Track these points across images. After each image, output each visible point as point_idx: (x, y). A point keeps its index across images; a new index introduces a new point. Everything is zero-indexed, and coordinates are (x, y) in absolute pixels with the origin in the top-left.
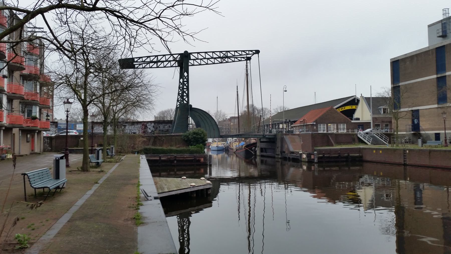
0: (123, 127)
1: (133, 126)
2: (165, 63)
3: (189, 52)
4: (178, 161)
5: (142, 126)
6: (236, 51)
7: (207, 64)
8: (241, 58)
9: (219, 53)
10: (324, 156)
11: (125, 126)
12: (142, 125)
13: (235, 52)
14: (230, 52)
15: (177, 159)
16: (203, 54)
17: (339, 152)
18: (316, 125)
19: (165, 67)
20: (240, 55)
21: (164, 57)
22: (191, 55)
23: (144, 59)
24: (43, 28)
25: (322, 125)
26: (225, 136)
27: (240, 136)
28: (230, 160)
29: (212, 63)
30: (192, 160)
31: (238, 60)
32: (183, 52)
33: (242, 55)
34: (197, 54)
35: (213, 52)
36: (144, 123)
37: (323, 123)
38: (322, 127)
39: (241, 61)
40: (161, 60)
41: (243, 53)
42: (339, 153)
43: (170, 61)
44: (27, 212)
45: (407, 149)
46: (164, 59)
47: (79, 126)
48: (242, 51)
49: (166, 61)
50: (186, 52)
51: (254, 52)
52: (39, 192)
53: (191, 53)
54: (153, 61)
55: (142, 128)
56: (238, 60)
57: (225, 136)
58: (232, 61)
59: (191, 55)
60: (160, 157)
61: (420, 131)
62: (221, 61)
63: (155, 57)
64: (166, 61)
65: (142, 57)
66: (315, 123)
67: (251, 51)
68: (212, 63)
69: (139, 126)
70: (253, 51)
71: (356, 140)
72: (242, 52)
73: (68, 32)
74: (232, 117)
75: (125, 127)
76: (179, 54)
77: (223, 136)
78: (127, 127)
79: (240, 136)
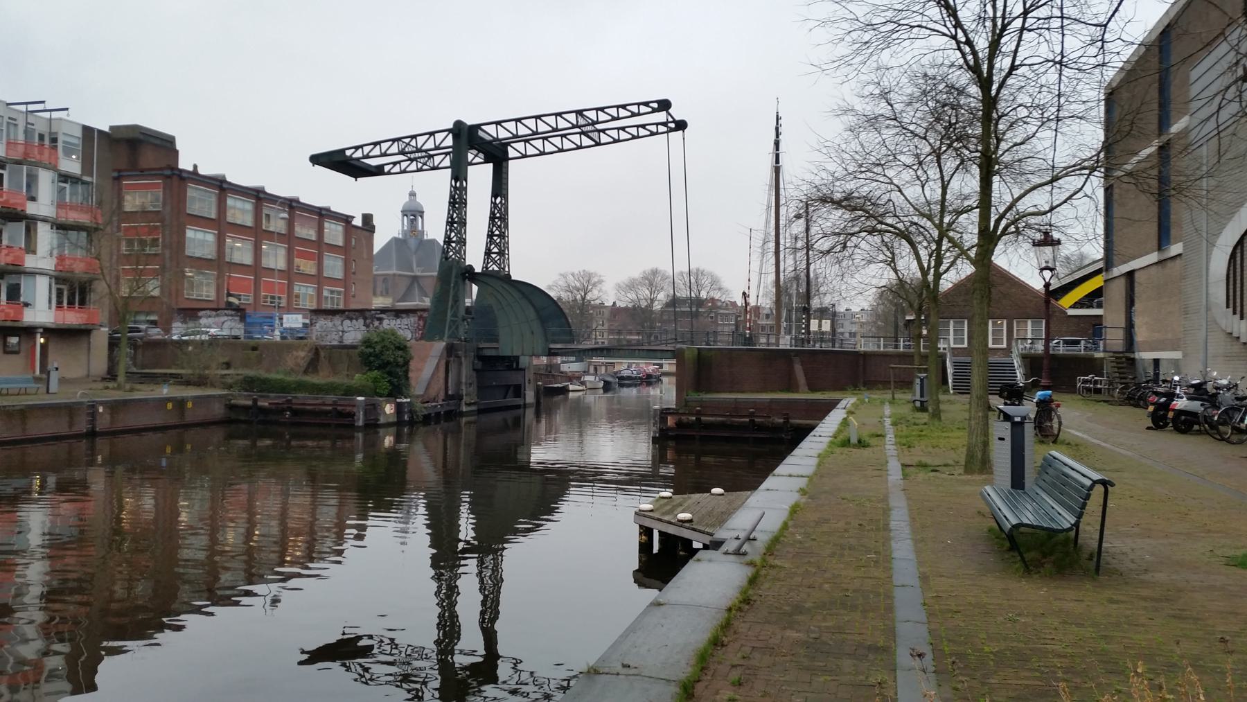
0: (376, 323)
1: (398, 321)
4: (295, 413)
5: (419, 320)
6: (602, 109)
7: (561, 150)
10: (698, 420)
11: (380, 320)
12: (417, 318)
13: (599, 112)
15: (294, 407)
16: (531, 123)
17: (751, 410)
20: (614, 119)
21: (432, 137)
24: (43, 102)
25: (1029, 322)
26: (564, 351)
27: (605, 352)
30: (329, 412)
33: (618, 118)
35: (538, 117)
36: (422, 313)
38: (1029, 328)
39: (657, 133)
42: (753, 413)
45: (102, 403)
47: (288, 318)
48: (618, 107)
51: (655, 105)
53: (478, 126)
55: (419, 325)
56: (649, 133)
57: (564, 351)
58: (630, 136)
60: (255, 401)
61: (1134, 352)
63: (391, 143)
65: (361, 147)
67: (646, 104)
69: (412, 319)
70: (651, 105)
72: (620, 109)
73: (1059, 52)
75: (380, 324)
76: (449, 131)
77: (560, 351)
78: (385, 322)
79: (605, 352)
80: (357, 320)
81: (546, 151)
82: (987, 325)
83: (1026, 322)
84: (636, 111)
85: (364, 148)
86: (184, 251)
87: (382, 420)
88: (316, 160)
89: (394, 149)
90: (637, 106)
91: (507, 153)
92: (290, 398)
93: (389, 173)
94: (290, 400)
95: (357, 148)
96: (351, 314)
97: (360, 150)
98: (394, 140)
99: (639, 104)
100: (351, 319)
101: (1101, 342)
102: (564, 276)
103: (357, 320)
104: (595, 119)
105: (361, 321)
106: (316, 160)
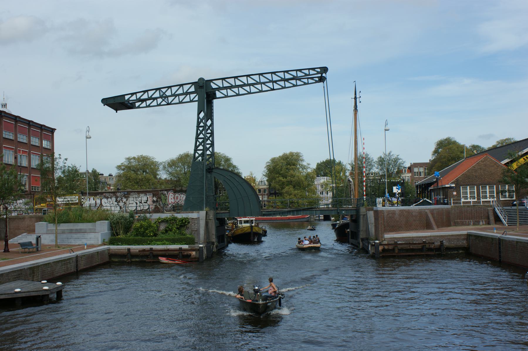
2: (148, 102)
3: (206, 79)
8: (308, 78)
9: (283, 73)
14: (264, 75)
18: (457, 189)
19: (181, 102)
22: (212, 83)
23: (139, 95)
28: (306, 244)
29: (258, 91)
31: (303, 83)
32: (197, 81)
34: (246, 77)
37: (472, 185)
39: (308, 84)
40: (153, 97)
41: (312, 72)
43: (156, 98)
44: (327, 296)
46: (145, 96)
48: (297, 70)
49: (149, 99)
50: (201, 79)
51: (319, 70)
52: (482, 264)
53: (211, 81)
54: (141, 98)
56: (303, 83)
58: (292, 85)
59: (212, 83)
62: (166, 102)
64: (149, 99)
65: (136, 93)
66: (453, 185)
68: (258, 91)
71: (492, 218)
72: (298, 72)
74: (414, 163)
75: (127, 200)
76: (193, 83)
80: (111, 198)
81: (240, 93)
82: (460, 187)
83: (494, 186)
84: (308, 73)
85: (137, 94)
86: (428, 163)
87: (198, 256)
88: (105, 101)
89: (157, 95)
90: (308, 70)
91: (215, 94)
92: (396, 241)
93: (139, 107)
94: (397, 242)
95: (132, 94)
96: (107, 195)
97: (135, 95)
98: (156, 89)
99: (309, 69)
100: (107, 198)
101: (357, 198)
102: (129, 159)
103: (111, 198)
104: (261, 76)
105: (114, 199)
106: (105, 101)
